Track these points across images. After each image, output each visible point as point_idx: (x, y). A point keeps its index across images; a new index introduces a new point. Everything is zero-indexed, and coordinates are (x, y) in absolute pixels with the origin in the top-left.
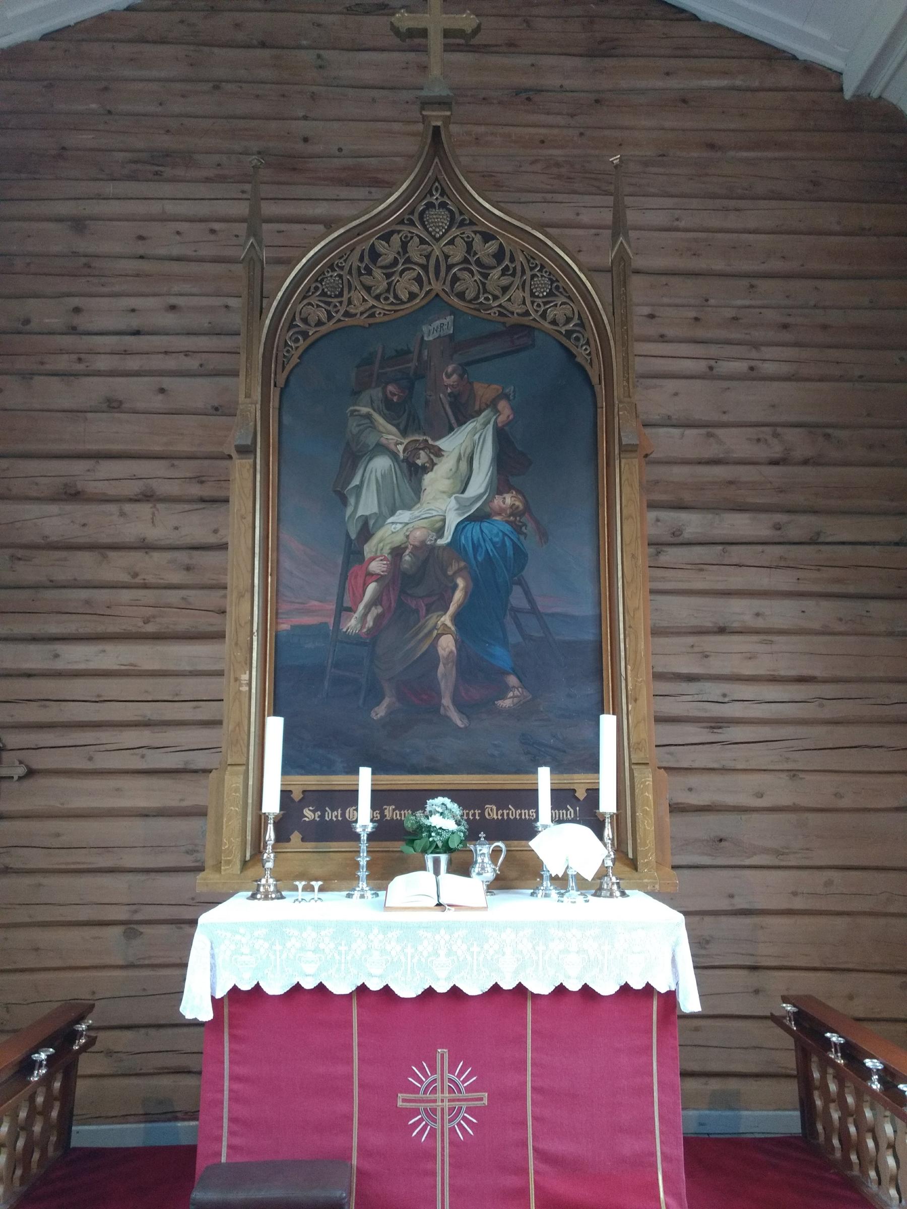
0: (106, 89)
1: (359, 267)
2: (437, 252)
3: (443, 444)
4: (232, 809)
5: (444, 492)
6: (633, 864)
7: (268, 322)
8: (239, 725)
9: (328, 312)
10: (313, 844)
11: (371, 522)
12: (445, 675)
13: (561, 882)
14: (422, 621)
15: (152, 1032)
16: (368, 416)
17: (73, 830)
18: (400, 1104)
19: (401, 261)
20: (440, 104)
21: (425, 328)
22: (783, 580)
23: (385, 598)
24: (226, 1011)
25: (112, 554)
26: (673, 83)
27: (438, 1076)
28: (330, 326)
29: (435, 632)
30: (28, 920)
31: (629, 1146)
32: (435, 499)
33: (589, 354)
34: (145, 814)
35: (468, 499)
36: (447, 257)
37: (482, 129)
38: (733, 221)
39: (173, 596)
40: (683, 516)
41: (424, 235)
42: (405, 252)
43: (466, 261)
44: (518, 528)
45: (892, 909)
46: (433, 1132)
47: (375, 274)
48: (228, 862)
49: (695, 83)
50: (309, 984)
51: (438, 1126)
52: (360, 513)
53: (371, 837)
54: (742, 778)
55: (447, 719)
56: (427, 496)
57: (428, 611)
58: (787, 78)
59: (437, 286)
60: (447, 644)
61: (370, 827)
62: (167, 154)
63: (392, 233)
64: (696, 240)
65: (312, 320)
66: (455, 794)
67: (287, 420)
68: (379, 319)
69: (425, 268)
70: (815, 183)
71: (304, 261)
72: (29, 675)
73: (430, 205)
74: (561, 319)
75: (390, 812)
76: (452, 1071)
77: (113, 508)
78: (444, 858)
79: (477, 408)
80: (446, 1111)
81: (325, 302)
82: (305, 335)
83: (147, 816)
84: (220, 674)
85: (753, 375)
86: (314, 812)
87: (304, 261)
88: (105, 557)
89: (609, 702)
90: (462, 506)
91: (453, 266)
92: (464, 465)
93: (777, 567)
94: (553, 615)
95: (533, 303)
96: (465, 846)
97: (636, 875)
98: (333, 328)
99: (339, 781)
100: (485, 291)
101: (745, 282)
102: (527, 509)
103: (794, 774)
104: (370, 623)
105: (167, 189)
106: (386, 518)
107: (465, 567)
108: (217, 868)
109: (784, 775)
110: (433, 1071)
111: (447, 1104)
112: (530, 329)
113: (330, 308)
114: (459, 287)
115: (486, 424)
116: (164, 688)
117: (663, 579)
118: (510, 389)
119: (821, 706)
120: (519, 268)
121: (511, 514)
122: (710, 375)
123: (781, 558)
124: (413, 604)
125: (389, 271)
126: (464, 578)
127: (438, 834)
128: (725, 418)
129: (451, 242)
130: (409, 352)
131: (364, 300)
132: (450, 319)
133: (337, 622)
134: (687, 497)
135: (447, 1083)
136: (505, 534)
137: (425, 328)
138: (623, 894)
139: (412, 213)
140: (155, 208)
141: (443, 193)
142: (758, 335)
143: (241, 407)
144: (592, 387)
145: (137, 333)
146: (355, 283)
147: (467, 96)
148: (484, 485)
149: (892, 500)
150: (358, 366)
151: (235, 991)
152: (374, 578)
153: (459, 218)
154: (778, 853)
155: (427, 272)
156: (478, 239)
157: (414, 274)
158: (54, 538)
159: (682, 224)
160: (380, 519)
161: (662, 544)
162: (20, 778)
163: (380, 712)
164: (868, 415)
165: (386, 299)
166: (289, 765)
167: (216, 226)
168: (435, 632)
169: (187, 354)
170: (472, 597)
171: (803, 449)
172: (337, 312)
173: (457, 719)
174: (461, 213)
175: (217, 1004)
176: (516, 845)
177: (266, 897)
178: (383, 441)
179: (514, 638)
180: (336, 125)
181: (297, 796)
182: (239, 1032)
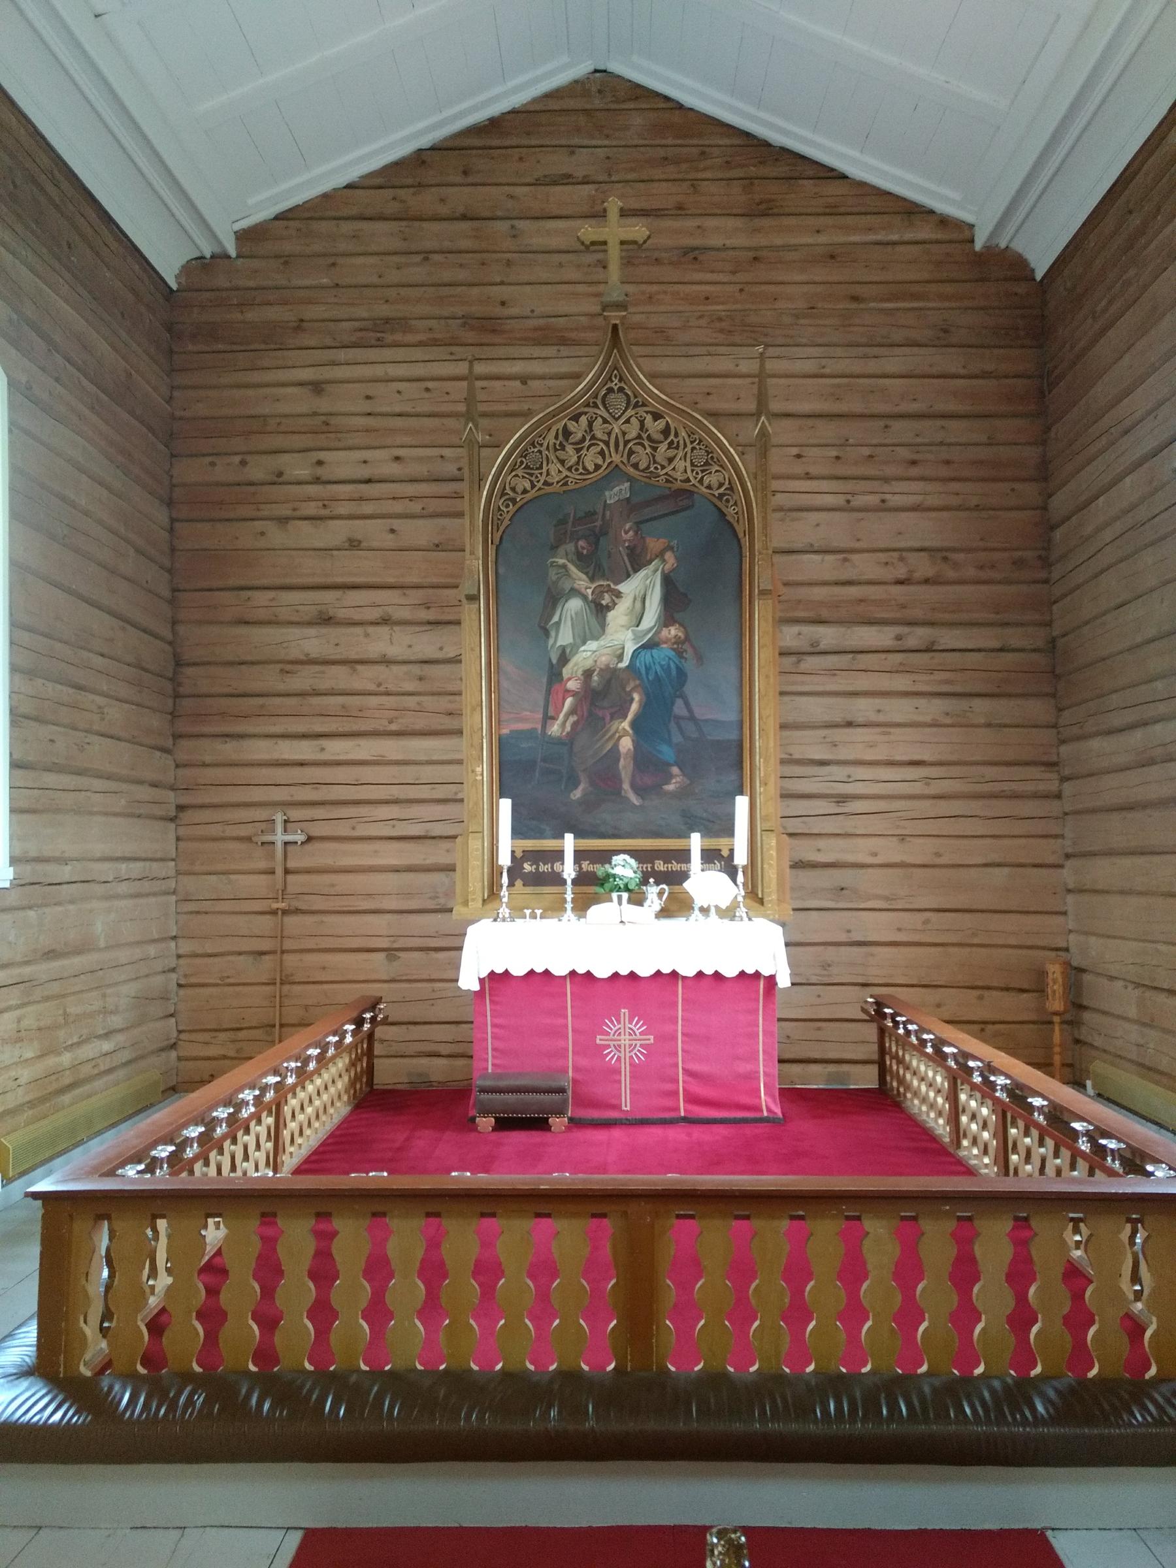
0: (334, 264)
1: (555, 444)
2: (617, 430)
3: (622, 587)
4: (474, 863)
5: (623, 626)
6: (761, 902)
7: (485, 493)
8: (476, 804)
9: (532, 482)
10: (532, 888)
11: (568, 651)
12: (625, 767)
13: (705, 911)
14: (608, 726)
15: (411, 1027)
16: (564, 566)
17: (344, 882)
18: (598, 1042)
19: (588, 438)
20: (617, 306)
21: (607, 493)
22: (902, 683)
23: (579, 708)
24: (487, 986)
25: (359, 667)
26: (822, 239)
27: (621, 1026)
28: (532, 494)
29: (617, 735)
30: (315, 947)
31: (743, 1067)
32: (616, 632)
33: (737, 513)
34: (396, 870)
35: (641, 631)
36: (624, 434)
37: (655, 288)
38: (872, 366)
39: (411, 701)
40: (821, 630)
41: (606, 415)
42: (591, 430)
43: (639, 437)
44: (680, 654)
45: (976, 941)
46: (619, 1059)
47: (567, 449)
48: (473, 900)
49: (842, 238)
51: (622, 1055)
52: (558, 644)
54: (860, 841)
55: (627, 799)
56: (610, 629)
57: (612, 719)
58: (925, 232)
59: (616, 458)
60: (626, 744)
61: (573, 875)
62: (387, 320)
63: (580, 414)
64: (839, 386)
65: (519, 489)
66: (633, 853)
67: (501, 571)
68: (571, 486)
69: (607, 443)
70: (946, 331)
71: (512, 441)
72: (302, 764)
73: (610, 390)
74: (715, 484)
75: (586, 866)
76: (630, 1022)
77: (358, 630)
78: (625, 896)
79: (648, 558)
80: (627, 1046)
81: (528, 474)
82: (514, 501)
83: (398, 871)
85: (883, 507)
86: (531, 865)
87: (512, 441)
88: (355, 670)
89: (747, 788)
91: (629, 441)
92: (638, 605)
93: (897, 672)
94: (706, 721)
95: (692, 471)
96: (640, 888)
97: (762, 908)
98: (536, 495)
99: (549, 844)
100: (655, 462)
101: (882, 423)
102: (687, 639)
103: (902, 838)
104: (568, 728)
105: (388, 354)
106: (578, 648)
107: (640, 685)
108: (466, 903)
109: (895, 839)
110: (619, 1022)
111: (627, 1042)
112: (691, 493)
113: (533, 479)
114: (633, 459)
115: (656, 571)
116: (409, 773)
117: (803, 683)
118: (674, 543)
119: (927, 784)
120: (682, 442)
121: (675, 643)
122: (847, 508)
123: (901, 664)
124: (600, 714)
125: (579, 446)
126: (638, 693)
127: (621, 879)
128: (858, 545)
129: (628, 421)
130: (595, 513)
131: (560, 471)
132: (627, 485)
133: (544, 726)
134: (825, 614)
135: (627, 1030)
136: (670, 659)
137: (607, 493)
138: (750, 919)
139: (596, 397)
140: (379, 371)
141: (621, 380)
142: (890, 471)
143: (468, 562)
144: (739, 541)
145: (369, 481)
146: (552, 457)
147: (641, 257)
148: (654, 620)
149: (998, 613)
150: (555, 526)
151: (492, 974)
152: (571, 694)
153: (633, 401)
154: (887, 899)
155: (608, 446)
156: (649, 418)
157: (599, 449)
158: (313, 656)
159: (827, 371)
160: (575, 648)
161: (803, 653)
162: (302, 843)
163: (577, 794)
164: (982, 539)
165: (577, 470)
166: (517, 832)
167: (430, 385)
168: (617, 735)
169: (411, 499)
170: (645, 706)
171: (924, 567)
172: (538, 482)
173: (634, 799)
174: (636, 397)
175: (481, 981)
176: (676, 888)
177: (504, 920)
178: (576, 586)
179: (677, 738)
180: (528, 288)
181: (519, 854)
182: (496, 999)
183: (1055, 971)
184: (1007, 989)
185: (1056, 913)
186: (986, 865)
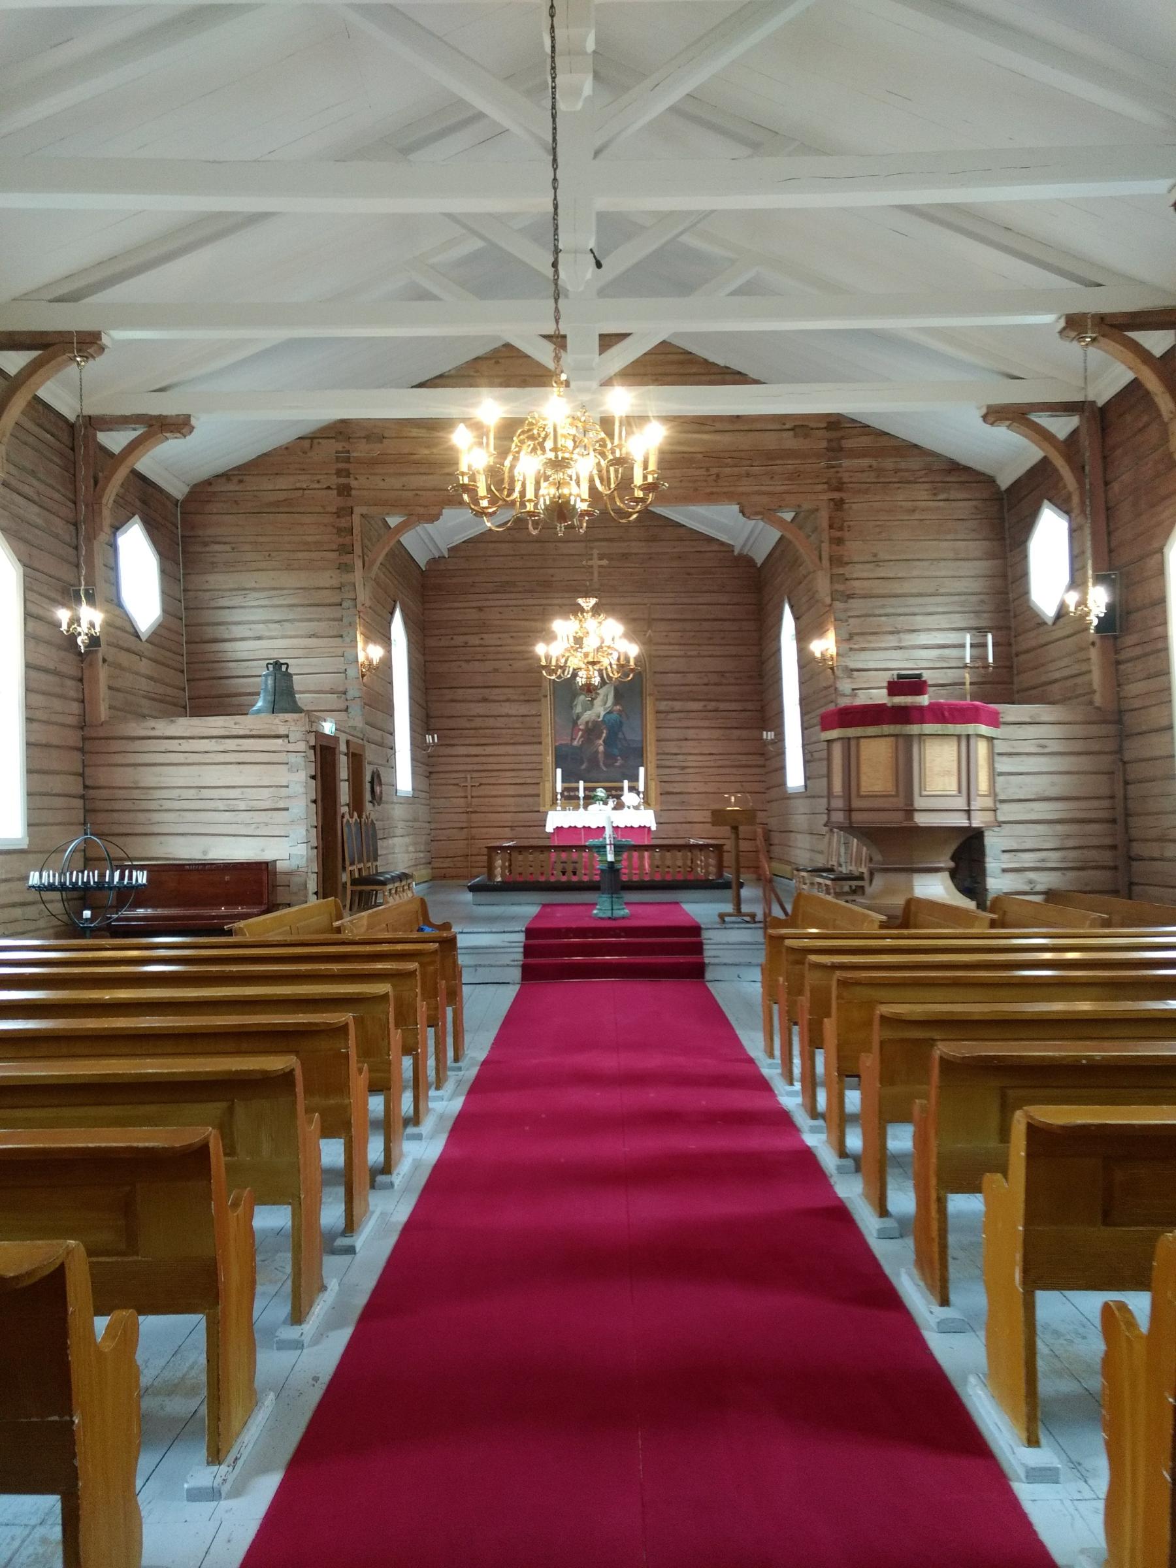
17: (499, 801)
22: (706, 723)
38: (693, 601)
39: (517, 731)
44: (621, 716)
50: (573, 825)
53: (584, 798)
60: (601, 748)
66: (604, 788)
77: (497, 704)
84: (541, 755)
90: (605, 710)
99: (573, 785)
103: (706, 782)
160: (582, 713)
163: (583, 767)
166: (563, 782)
173: (605, 769)
183: (760, 831)
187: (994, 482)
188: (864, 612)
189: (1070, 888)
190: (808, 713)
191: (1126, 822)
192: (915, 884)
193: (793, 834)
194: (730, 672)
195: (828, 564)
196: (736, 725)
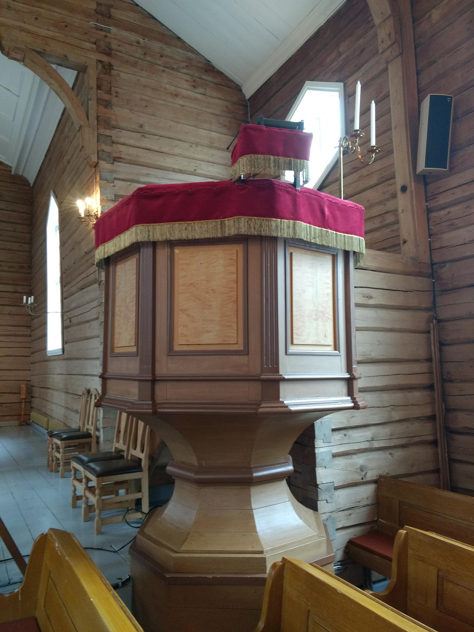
183: (23, 386)
184: (11, 393)
185: (28, 370)
186: (6, 356)
187: (241, 91)
188: (129, 177)
189: (398, 472)
190: (67, 284)
191: (443, 388)
192: (253, 506)
193: (49, 391)
194: (5, 262)
195: (96, 122)
196: (8, 303)
